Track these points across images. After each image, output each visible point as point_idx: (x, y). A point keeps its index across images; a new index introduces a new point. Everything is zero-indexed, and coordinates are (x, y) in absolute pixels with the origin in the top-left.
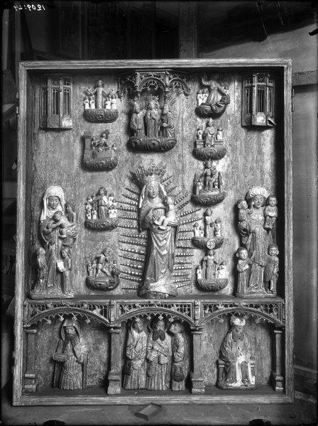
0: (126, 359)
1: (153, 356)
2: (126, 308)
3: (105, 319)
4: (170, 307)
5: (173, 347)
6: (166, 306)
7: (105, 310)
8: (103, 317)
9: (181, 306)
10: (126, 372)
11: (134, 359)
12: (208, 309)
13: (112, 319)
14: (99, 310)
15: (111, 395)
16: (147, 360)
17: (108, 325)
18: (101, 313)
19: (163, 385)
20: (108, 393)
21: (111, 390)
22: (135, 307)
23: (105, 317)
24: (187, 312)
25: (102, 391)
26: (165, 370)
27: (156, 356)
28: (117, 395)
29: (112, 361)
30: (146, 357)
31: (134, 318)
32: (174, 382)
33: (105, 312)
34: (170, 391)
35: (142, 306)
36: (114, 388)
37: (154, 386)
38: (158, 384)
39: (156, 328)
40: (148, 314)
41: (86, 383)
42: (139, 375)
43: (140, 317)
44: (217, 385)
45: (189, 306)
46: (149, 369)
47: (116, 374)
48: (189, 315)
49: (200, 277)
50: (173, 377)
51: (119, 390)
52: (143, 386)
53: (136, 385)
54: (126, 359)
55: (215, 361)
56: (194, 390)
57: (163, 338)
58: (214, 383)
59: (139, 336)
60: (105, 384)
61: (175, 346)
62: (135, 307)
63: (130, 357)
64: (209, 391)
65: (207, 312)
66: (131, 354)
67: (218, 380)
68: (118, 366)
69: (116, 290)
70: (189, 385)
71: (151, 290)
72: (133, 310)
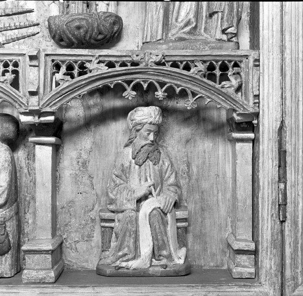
12: (63, 69)
65: (59, 76)
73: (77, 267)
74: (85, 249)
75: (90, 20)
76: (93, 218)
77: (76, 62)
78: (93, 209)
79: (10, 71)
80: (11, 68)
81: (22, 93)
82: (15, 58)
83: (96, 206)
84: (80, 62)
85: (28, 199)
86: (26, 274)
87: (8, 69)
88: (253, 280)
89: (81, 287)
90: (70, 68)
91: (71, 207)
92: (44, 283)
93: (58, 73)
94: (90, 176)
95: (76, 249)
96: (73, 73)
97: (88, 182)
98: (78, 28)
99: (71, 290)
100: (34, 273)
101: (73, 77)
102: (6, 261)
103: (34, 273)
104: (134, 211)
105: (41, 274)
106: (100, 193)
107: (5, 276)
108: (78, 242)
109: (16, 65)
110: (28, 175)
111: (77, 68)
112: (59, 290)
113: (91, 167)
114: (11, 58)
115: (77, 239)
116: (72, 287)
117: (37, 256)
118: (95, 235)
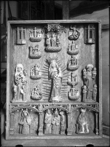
0: (44, 123)
1: (54, 123)
4: (59, 106)
5: (61, 119)
6: (58, 105)
7: (37, 107)
8: (36, 109)
9: (64, 105)
10: (44, 128)
11: (47, 124)
12: (73, 106)
13: (40, 110)
14: (22, 56)
16: (52, 124)
18: (36, 108)
22: (47, 106)
23: (37, 109)
24: (66, 107)
31: (47, 109)
36: (40, 134)
45: (66, 105)
46: (52, 127)
48: (66, 108)
52: (50, 133)
54: (44, 123)
56: (68, 134)
62: (47, 106)
65: (72, 107)
70: (66, 132)
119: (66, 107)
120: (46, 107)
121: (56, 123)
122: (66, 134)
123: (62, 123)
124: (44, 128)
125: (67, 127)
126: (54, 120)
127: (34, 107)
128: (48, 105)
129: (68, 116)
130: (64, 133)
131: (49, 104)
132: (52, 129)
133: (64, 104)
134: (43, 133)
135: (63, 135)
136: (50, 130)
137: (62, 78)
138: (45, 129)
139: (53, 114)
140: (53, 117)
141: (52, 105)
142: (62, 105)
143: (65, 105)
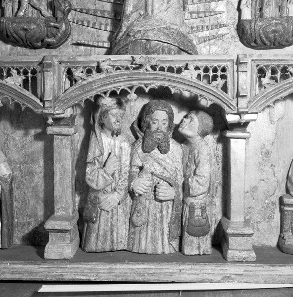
0: (82, 187)
1: (142, 185)
2: (77, 74)
3: (33, 97)
4: (179, 71)
5: (186, 166)
6: (171, 70)
7: (34, 79)
8: (28, 93)
9: (206, 70)
10: (84, 221)
11: (104, 191)
12: (269, 74)
13: (48, 96)
14: (21, 79)
15: (51, 261)
16: (132, 193)
17: (39, 111)
18: (25, 83)
19: (168, 247)
20: (46, 256)
21: (52, 250)
22: (99, 70)
23: (34, 92)
24: (220, 82)
25: (32, 250)
26: (168, 212)
27: (148, 183)
28: (64, 260)
29: (57, 193)
30: (129, 187)
31: (97, 97)
32: (188, 238)
33: (32, 82)
34: (180, 256)
35: (118, 69)
36: (60, 248)
37: (145, 245)
38: (154, 240)
39: (149, 127)
40: (131, 88)
41: (51, 232)
42: (113, 226)
43: (113, 94)
44: (279, 246)
45: (224, 70)
46: (133, 211)
47: (64, 219)
48: (225, 88)
49: (247, 15)
50: (183, 228)
51: (69, 251)
52: (122, 247)
53: (108, 242)
54: (82, 187)
55: (275, 199)
56: (230, 254)
57: (164, 150)
58: (273, 242)
59: (114, 147)
60: (37, 240)
61: (191, 163)
62: (99, 70)
63: (94, 186)
64: (264, 256)
65: (265, 81)
66: (95, 177)
67: (281, 238)
68: (67, 201)
69: (63, 48)
70: (220, 241)
71: (138, 36)
72: (95, 76)
73: (258, 244)
74: (266, 228)
75: (286, 25)
76: (274, 202)
77: (279, 66)
78: (274, 194)
79: (219, 76)
80: (219, 73)
81: (230, 95)
82: (223, 64)
83: (277, 191)
84: (282, 66)
85: (216, 184)
86: (230, 254)
87: (216, 73)
88: (152, 196)
89: (280, 266)
90: (274, 71)
91: (254, 191)
92: (247, 262)
93: (264, 77)
94: (272, 165)
95: (258, 228)
96: (276, 77)
97: (271, 170)
98: (274, 31)
99: (271, 268)
100: (237, 254)
101: (276, 81)
102: (206, 240)
103: (237, 254)
104: (57, 121)
105: (244, 254)
106: (281, 178)
107: (206, 253)
108: (260, 222)
109: (224, 70)
110: (216, 164)
111: (279, 72)
112: (261, 268)
113: (273, 156)
114: (219, 64)
115: (259, 220)
116: (272, 266)
117: (239, 239)
118: (275, 216)
119: (223, 77)
120: (90, 79)
121: (155, 189)
122: (218, 254)
123: (193, 183)
124: (84, 221)
125: (226, 212)
126: (147, 166)
127: (15, 81)
128: (104, 66)
129: (237, 147)
130: (206, 244)
131: (108, 62)
132: (130, 220)
133: (209, 64)
134: (80, 246)
135: (200, 258)
136: (122, 230)
137: (173, 200)
138: (90, 221)
139: (137, 138)
140: (140, 150)
141: (127, 68)
142: (197, 68)
143: (215, 70)
